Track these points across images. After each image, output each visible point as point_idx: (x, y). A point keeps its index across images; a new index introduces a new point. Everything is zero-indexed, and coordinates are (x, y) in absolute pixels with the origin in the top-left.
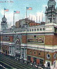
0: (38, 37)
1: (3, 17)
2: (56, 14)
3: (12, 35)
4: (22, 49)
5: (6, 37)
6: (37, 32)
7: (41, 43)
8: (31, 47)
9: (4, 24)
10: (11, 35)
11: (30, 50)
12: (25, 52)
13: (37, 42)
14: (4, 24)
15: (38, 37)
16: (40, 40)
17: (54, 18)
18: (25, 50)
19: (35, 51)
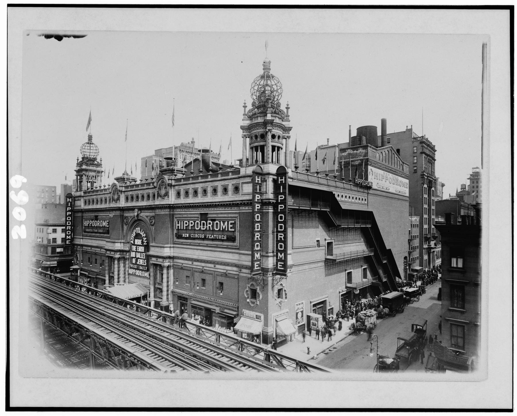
0: (214, 220)
1: (87, 141)
2: (287, 130)
3: (166, 212)
4: (156, 265)
5: (204, 217)
6: (209, 199)
7: (104, 233)
8: (91, 247)
9: (91, 168)
10: (158, 212)
11: (188, 273)
12: (165, 280)
13: (205, 239)
14: (91, 168)
15: (214, 220)
16: (223, 230)
17: (273, 147)
18: (165, 271)
19: (204, 276)
